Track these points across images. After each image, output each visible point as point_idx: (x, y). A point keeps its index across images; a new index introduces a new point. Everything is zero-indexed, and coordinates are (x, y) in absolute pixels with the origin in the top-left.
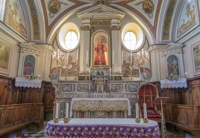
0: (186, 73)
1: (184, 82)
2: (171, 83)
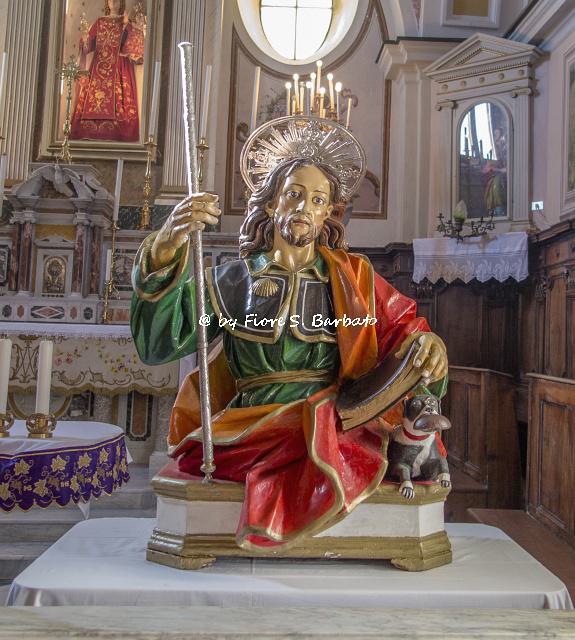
0: (538, 205)
1: (518, 248)
2: (460, 252)
